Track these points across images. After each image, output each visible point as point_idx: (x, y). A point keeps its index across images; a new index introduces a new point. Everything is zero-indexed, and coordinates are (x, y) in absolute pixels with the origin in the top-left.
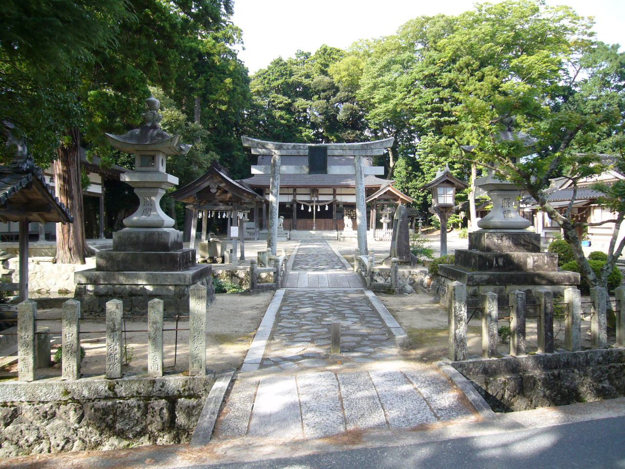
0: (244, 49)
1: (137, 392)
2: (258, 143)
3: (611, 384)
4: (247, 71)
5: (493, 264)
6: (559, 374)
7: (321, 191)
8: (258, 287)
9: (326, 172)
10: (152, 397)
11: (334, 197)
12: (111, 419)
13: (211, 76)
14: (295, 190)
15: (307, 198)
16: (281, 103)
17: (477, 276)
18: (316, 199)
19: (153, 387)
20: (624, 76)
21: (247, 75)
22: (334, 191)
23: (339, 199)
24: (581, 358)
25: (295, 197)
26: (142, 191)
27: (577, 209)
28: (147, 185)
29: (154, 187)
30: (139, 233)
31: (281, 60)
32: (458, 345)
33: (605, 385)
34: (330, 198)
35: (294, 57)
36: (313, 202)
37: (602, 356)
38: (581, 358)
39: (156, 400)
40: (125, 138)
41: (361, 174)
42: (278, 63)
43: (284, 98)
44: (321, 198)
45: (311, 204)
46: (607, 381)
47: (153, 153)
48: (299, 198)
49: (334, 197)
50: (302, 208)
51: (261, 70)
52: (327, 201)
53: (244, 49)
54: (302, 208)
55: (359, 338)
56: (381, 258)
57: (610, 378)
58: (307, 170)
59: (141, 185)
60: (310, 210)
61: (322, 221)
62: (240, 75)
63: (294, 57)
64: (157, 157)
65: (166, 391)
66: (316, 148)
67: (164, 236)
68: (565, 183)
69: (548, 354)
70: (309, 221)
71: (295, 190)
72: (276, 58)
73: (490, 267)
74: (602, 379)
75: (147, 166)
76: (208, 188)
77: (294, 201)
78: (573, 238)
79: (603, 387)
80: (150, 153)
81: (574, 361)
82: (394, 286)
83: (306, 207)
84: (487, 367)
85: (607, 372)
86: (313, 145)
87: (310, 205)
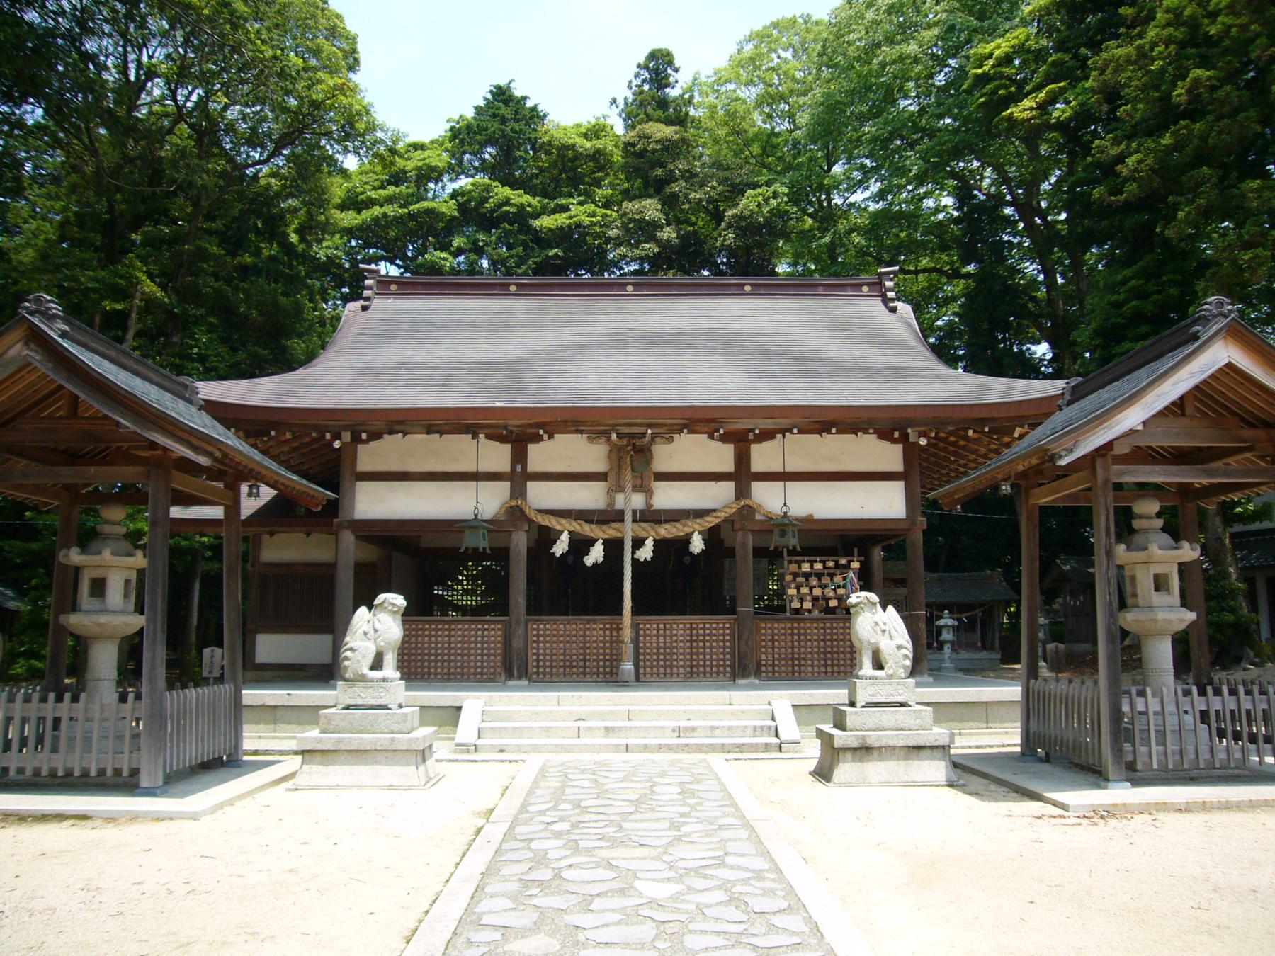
7: (668, 456)
11: (742, 492)
14: (519, 456)
15: (589, 496)
18: (638, 501)
20: (9, 521)
22: (742, 459)
23: (770, 499)
25: (518, 491)
27: (145, 782)
34: (719, 496)
36: (619, 516)
44: (668, 496)
45: (611, 532)
48: (542, 496)
49: (742, 492)
52: (700, 514)
55: (497, 936)
56: (746, 869)
61: (676, 630)
68: (564, 857)
71: (519, 456)
77: (515, 514)
83: (581, 545)
87: (601, 533)
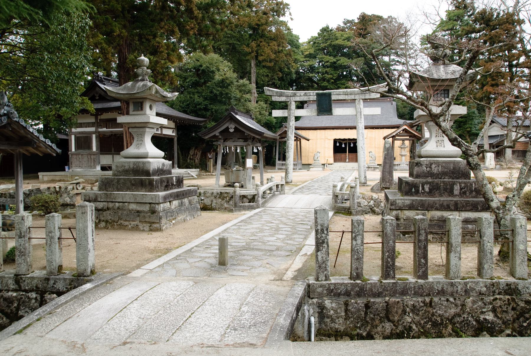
0: (292, 19)
1: (36, 287)
2: (277, 92)
3: (496, 316)
4: (297, 38)
5: (419, 190)
6: (431, 302)
8: (241, 206)
9: (332, 114)
10: (48, 291)
12: (15, 307)
13: (261, 42)
16: (327, 62)
17: (400, 201)
19: (48, 284)
21: (298, 41)
24: (459, 287)
26: (135, 130)
28: (137, 125)
29: (144, 125)
30: (130, 162)
31: (328, 28)
32: (320, 267)
33: (487, 317)
35: (342, 25)
37: (486, 286)
38: (459, 287)
39: (49, 294)
40: (119, 89)
41: (361, 114)
42: (325, 30)
43: (330, 58)
46: (491, 313)
47: (141, 100)
50: (338, 145)
51: (312, 37)
53: (292, 19)
54: (338, 145)
57: (494, 310)
58: (315, 113)
59: (133, 125)
60: (343, 146)
62: (293, 42)
63: (342, 25)
64: (144, 104)
65: (58, 288)
66: (322, 94)
67: (146, 165)
69: (419, 281)
70: (343, 155)
72: (324, 26)
73: (417, 193)
74: (484, 310)
75: (138, 110)
76: (227, 128)
78: (475, 165)
79: (485, 319)
80: (139, 100)
81: (450, 289)
82: (352, 208)
84: (349, 289)
85: (490, 303)
86: (321, 92)
87: (343, 142)
